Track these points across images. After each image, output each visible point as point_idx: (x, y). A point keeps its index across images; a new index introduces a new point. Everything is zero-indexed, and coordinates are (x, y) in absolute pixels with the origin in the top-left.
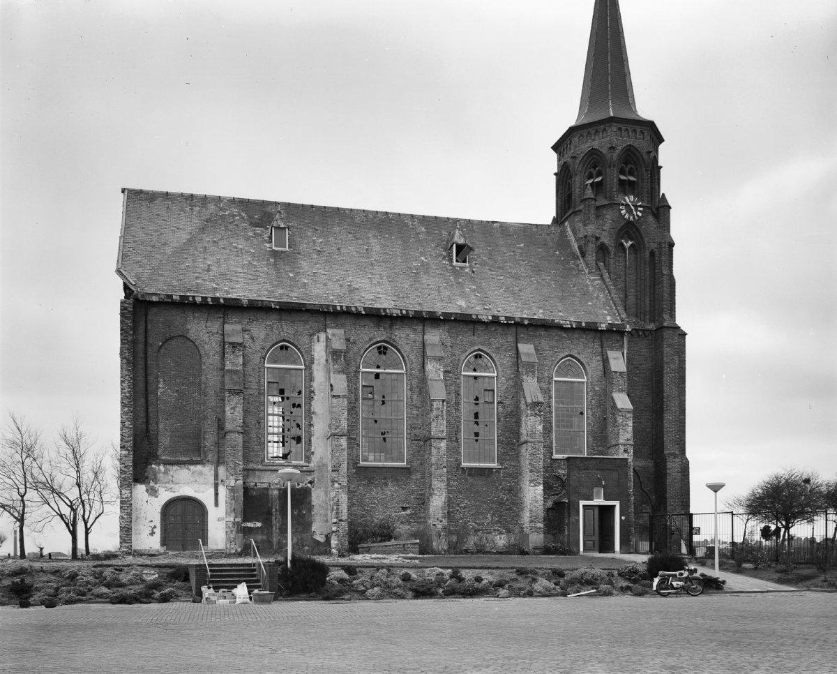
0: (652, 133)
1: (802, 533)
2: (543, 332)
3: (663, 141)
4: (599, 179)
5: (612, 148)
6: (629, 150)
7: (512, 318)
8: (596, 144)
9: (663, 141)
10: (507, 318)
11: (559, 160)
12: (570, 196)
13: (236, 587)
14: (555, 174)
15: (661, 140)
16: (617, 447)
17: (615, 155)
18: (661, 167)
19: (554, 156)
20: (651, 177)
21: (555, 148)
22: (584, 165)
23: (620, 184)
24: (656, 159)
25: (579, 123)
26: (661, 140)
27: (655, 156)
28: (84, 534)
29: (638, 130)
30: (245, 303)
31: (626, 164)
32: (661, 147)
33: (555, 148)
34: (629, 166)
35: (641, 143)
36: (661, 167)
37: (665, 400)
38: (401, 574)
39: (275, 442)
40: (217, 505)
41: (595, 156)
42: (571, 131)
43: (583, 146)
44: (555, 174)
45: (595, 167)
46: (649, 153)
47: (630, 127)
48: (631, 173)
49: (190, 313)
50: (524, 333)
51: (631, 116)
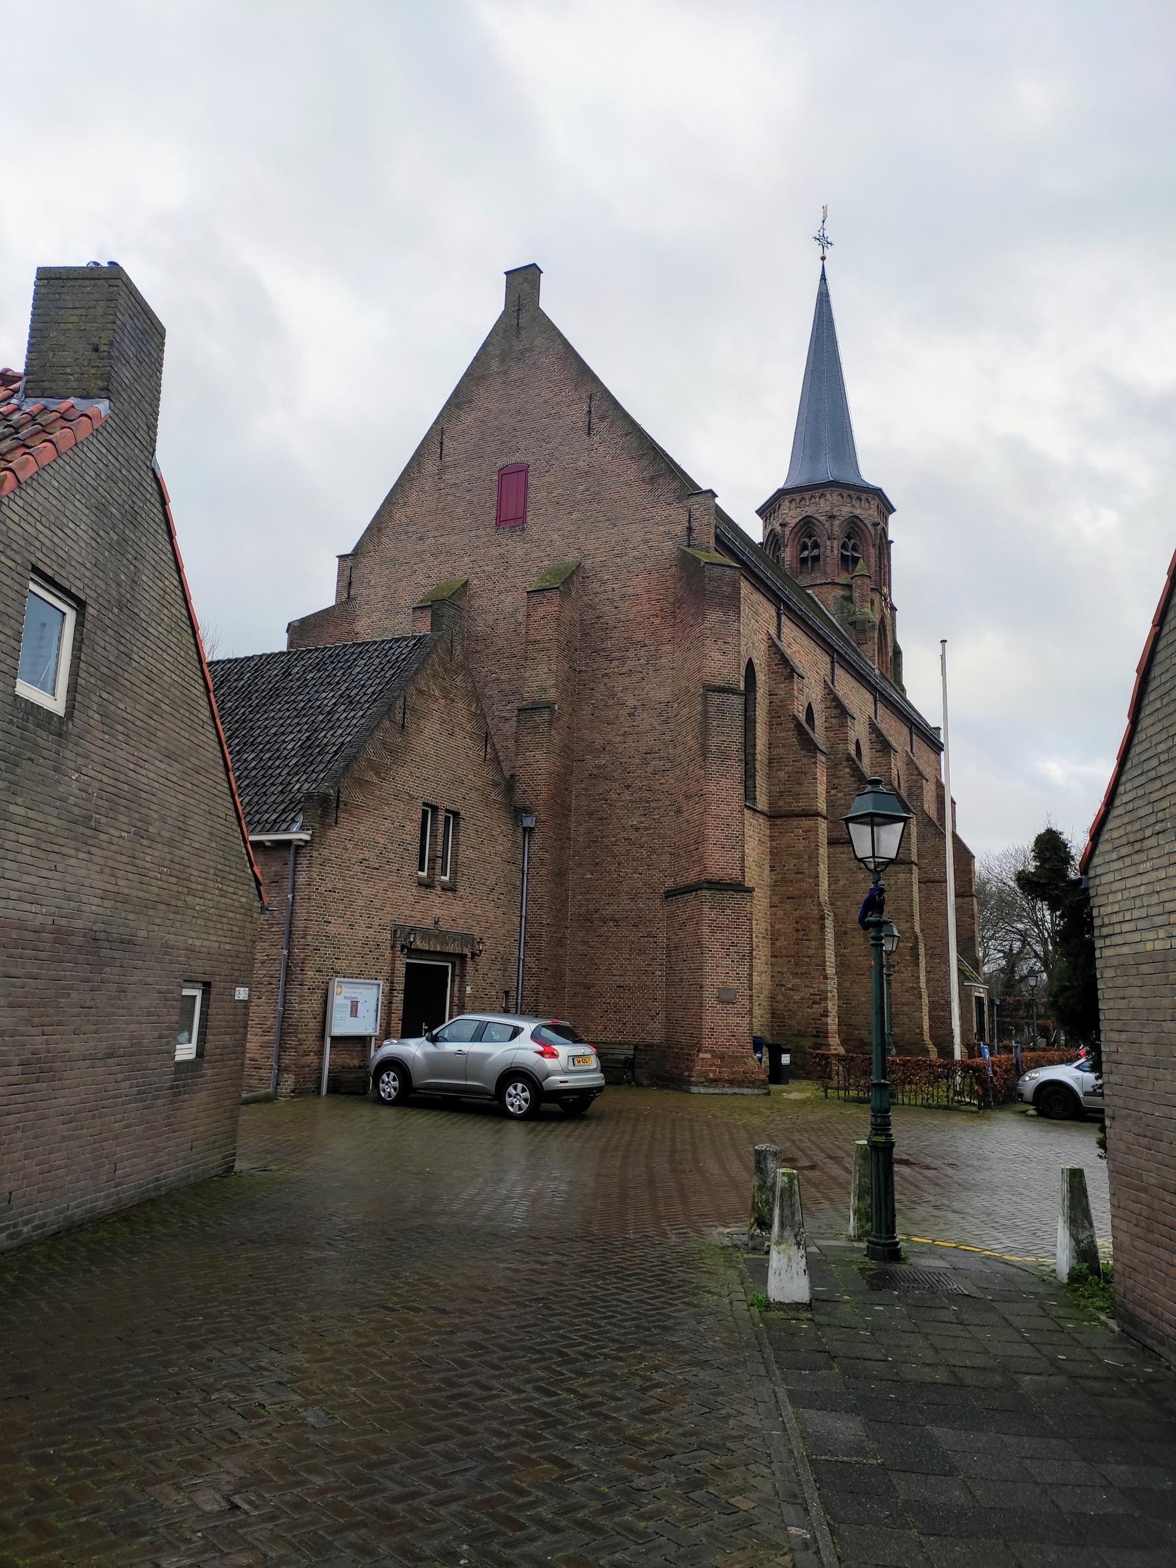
1: (1111, 1004)
5: (832, 517)
6: (853, 522)
8: (810, 511)
11: (765, 528)
15: (891, 510)
16: (806, 823)
17: (788, 530)
21: (761, 512)
24: (884, 532)
25: (789, 486)
26: (891, 510)
28: (1126, 722)
29: (854, 497)
31: (849, 537)
32: (892, 518)
34: (853, 541)
35: (867, 512)
39: (371, 730)
40: (858, 743)
41: (71, 616)
42: (781, 494)
43: (791, 515)
46: (876, 525)
47: (807, 495)
48: (854, 548)
51: (852, 480)
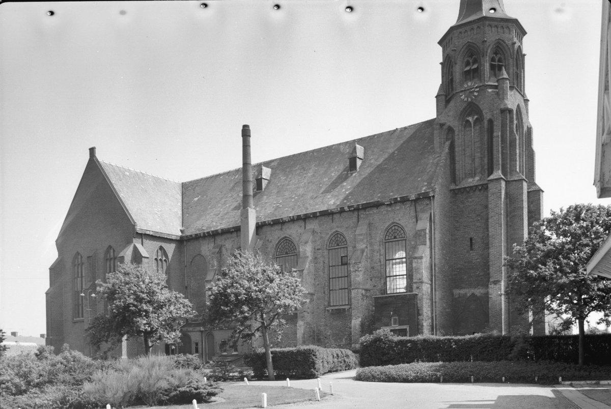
0: (515, 27)
2: (375, 210)
3: (526, 33)
4: (475, 66)
7: (353, 206)
9: (526, 33)
10: (349, 207)
11: (444, 52)
12: (452, 80)
13: (536, 195)
14: (441, 63)
18: (525, 55)
19: (440, 49)
20: (517, 63)
21: (440, 43)
22: (447, 68)
23: (491, 66)
27: (519, 46)
30: (220, 231)
31: (496, 53)
33: (440, 43)
34: (499, 56)
36: (525, 55)
37: (490, 239)
38: (543, 267)
42: (452, 29)
44: (441, 63)
45: (471, 56)
49: (201, 242)
50: (363, 214)
